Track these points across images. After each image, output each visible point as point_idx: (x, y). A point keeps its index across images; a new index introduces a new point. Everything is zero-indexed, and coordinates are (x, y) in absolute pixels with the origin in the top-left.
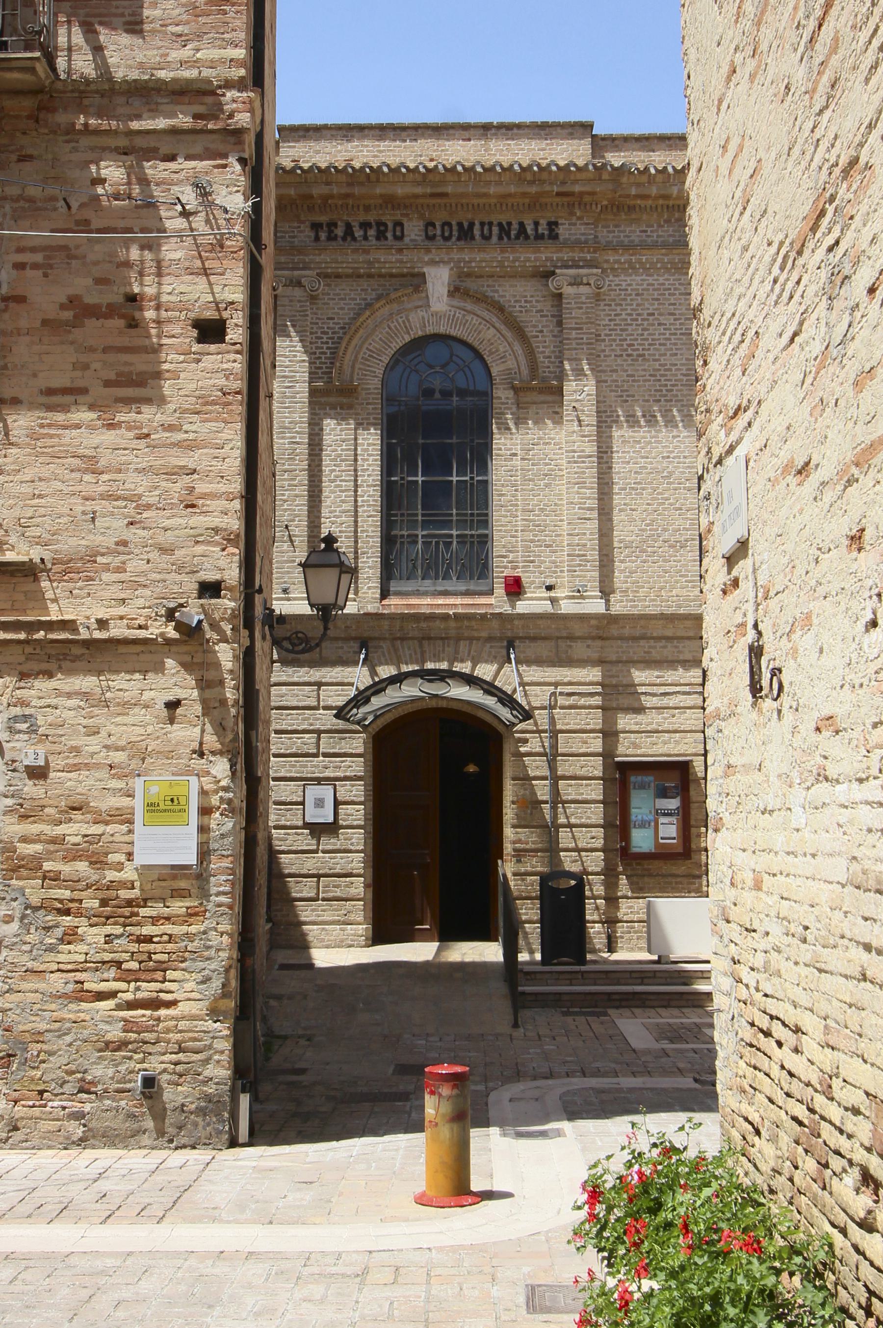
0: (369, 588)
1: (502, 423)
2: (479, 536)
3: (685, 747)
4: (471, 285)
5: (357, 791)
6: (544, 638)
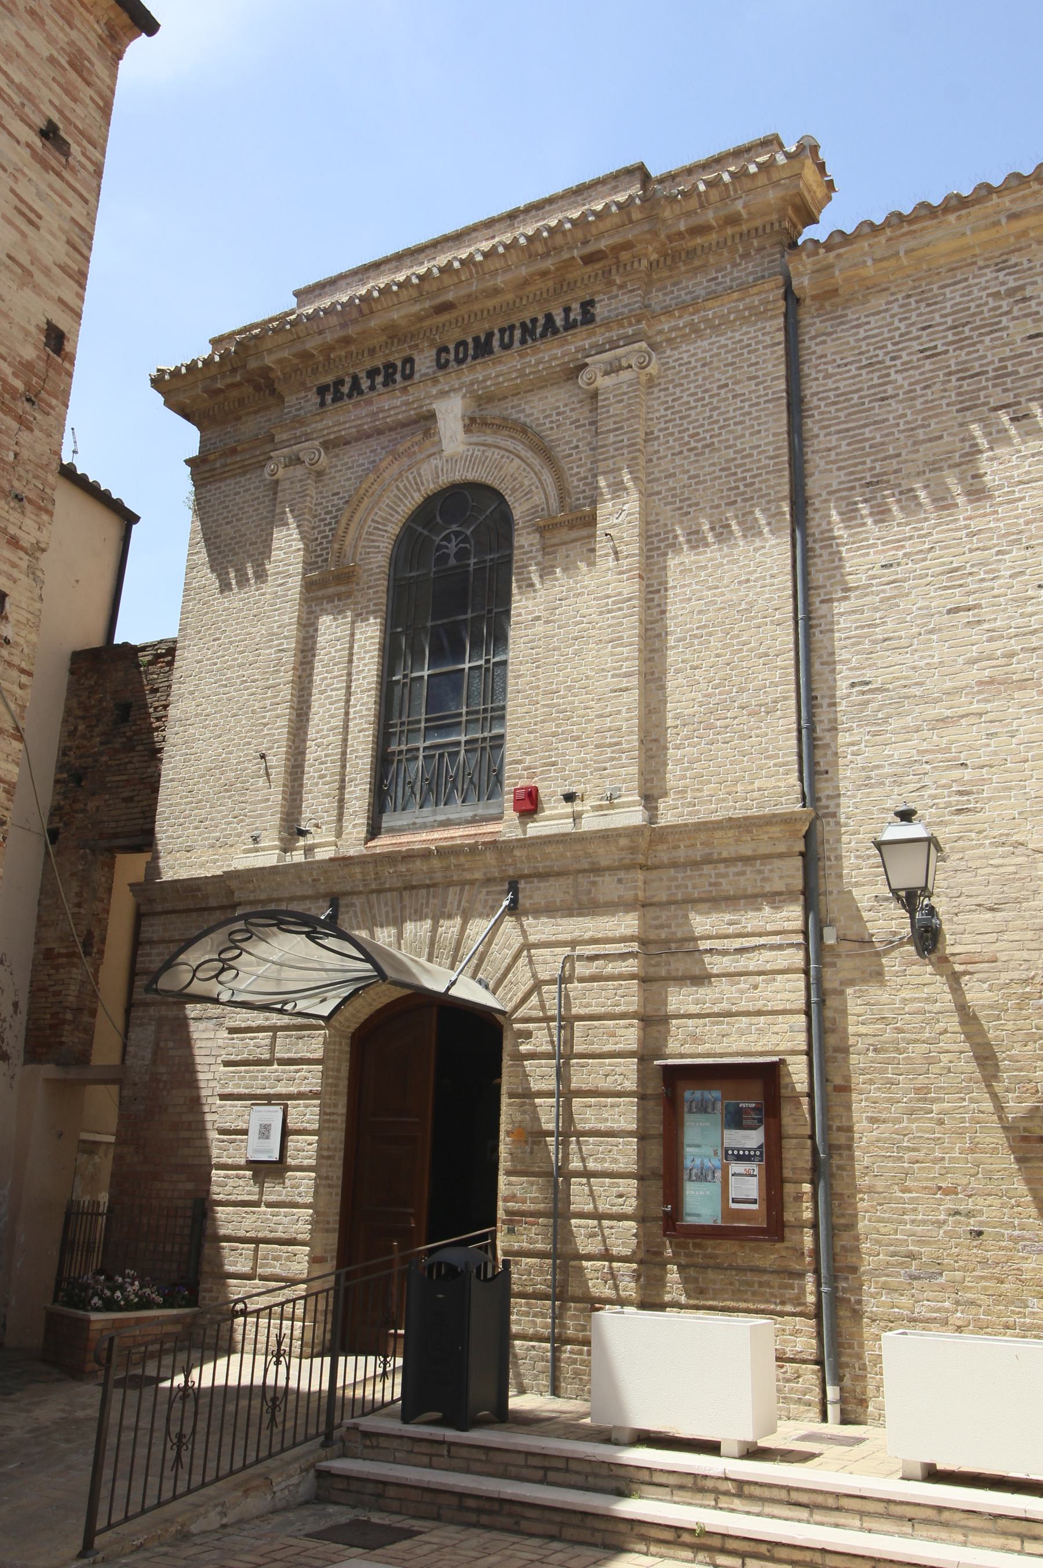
0: (354, 826)
1: (523, 580)
2: (492, 738)
3: (775, 1039)
4: (492, 411)
5: (306, 1115)
6: (559, 874)
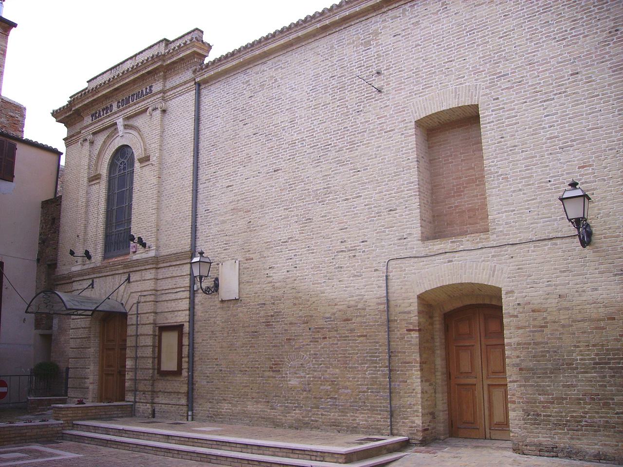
4: (113, 129)
